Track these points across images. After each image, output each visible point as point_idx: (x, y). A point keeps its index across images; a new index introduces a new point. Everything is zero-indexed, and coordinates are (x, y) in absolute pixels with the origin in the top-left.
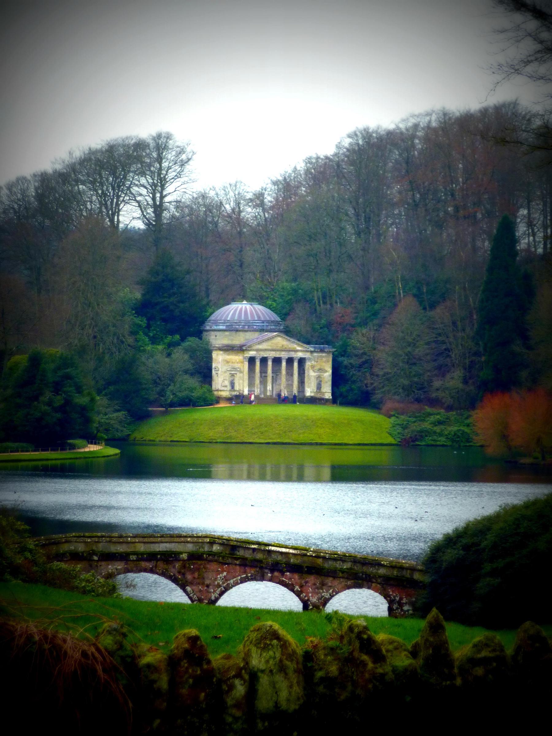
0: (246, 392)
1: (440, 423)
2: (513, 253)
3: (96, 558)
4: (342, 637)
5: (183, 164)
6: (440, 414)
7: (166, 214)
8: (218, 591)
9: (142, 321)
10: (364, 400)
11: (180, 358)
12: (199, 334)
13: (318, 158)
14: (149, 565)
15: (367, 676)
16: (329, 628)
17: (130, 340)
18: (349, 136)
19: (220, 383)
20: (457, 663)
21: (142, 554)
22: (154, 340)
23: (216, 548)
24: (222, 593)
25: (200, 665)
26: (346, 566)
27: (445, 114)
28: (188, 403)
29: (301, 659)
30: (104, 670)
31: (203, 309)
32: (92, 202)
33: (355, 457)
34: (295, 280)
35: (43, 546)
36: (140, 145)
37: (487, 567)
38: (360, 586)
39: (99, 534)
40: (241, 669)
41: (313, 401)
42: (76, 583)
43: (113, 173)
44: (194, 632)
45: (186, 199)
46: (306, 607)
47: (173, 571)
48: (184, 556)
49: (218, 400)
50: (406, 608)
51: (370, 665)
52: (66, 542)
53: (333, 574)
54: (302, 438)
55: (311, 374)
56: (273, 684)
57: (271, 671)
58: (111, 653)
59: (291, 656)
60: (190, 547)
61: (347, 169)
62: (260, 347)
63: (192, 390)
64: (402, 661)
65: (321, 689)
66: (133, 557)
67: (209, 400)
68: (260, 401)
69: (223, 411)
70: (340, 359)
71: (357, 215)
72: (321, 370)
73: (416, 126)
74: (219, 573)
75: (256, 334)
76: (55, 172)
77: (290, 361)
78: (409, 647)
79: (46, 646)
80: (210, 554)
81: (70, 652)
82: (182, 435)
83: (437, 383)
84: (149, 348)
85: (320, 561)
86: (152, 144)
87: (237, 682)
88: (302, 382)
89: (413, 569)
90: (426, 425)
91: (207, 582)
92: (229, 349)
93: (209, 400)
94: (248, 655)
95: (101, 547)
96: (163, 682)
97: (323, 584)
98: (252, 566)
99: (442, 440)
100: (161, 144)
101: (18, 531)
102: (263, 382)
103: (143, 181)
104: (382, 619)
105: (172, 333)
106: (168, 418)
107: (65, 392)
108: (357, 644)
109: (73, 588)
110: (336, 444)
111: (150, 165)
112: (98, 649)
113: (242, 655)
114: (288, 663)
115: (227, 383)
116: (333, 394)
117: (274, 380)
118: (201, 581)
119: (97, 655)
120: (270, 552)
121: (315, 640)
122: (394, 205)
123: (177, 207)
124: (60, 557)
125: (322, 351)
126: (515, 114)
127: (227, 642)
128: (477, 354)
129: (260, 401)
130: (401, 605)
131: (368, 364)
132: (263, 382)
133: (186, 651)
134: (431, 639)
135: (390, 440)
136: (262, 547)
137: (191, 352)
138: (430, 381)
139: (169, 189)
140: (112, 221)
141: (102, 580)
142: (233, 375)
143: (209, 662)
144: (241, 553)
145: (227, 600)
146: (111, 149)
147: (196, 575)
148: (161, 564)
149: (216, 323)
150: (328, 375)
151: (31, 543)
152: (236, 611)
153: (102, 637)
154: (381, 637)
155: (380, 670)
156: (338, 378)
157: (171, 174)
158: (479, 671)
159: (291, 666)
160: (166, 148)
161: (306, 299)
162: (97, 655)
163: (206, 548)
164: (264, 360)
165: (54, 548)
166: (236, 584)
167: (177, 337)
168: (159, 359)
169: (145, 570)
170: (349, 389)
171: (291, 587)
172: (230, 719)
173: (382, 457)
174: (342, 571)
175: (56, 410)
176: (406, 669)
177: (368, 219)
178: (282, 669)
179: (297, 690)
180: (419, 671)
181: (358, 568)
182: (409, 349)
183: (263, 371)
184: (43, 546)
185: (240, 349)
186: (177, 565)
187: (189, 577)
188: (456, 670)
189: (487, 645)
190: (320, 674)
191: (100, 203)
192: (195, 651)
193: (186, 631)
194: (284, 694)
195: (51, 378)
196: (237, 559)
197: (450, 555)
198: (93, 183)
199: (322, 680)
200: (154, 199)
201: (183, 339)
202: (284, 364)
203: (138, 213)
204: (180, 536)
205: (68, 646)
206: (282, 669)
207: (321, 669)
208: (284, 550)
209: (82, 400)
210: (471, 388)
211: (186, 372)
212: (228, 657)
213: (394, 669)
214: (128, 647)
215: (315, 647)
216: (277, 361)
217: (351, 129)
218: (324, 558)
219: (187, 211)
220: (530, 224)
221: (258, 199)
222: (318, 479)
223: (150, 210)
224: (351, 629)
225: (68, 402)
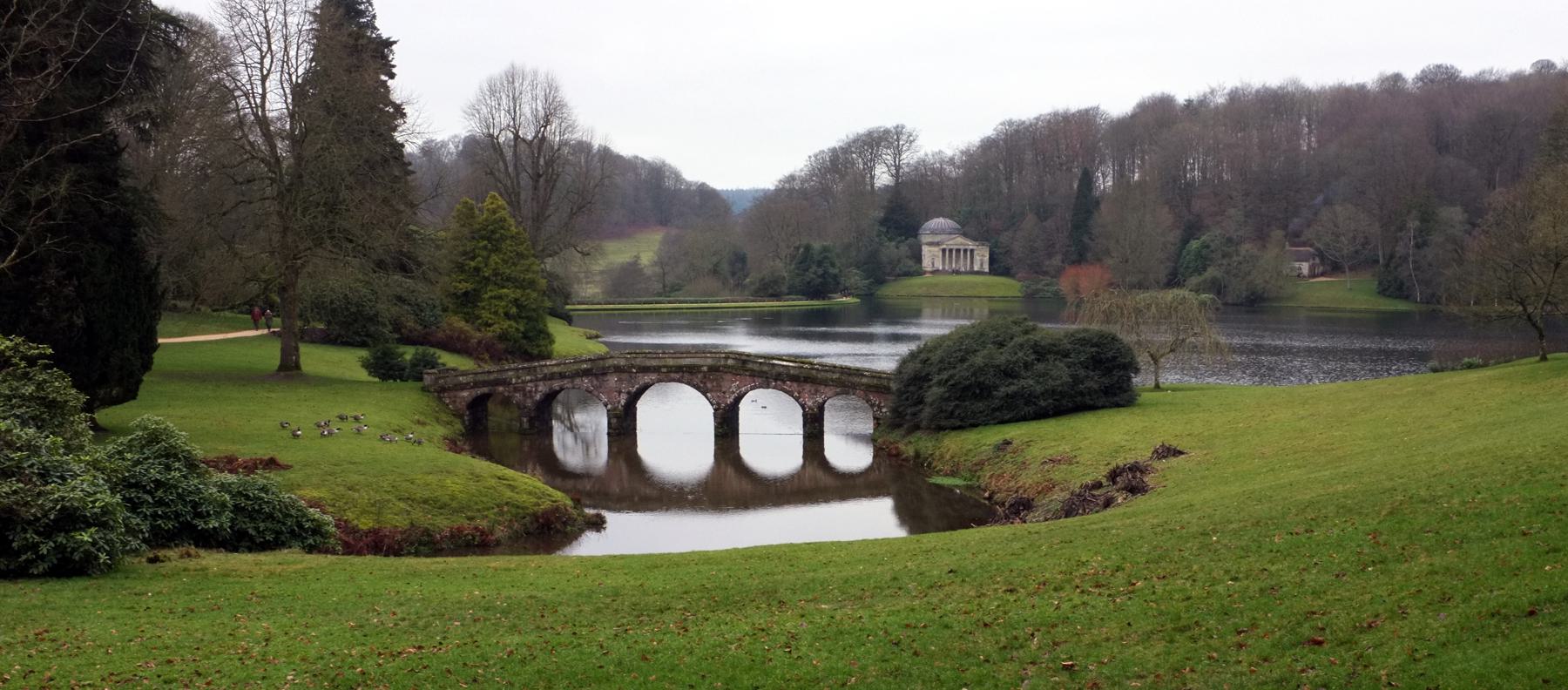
6: (1048, 279)
10: (1007, 272)
11: (904, 249)
12: (916, 236)
14: (677, 376)
19: (926, 263)
22: (891, 240)
23: (730, 362)
26: (835, 376)
28: (908, 274)
36: (887, 132)
37: (936, 379)
41: (978, 273)
53: (825, 382)
55: (977, 258)
60: (709, 362)
67: (920, 273)
69: (928, 278)
92: (931, 244)
93: (920, 273)
95: (638, 362)
97: (817, 391)
100: (899, 131)
129: (966, 273)
131: (1008, 252)
137: (910, 247)
144: (750, 366)
146: (870, 134)
150: (987, 258)
156: (992, 261)
168: (892, 250)
170: (998, 266)
171: (790, 393)
185: (938, 244)
209: (833, 271)
216: (958, 251)
217: (1001, 120)
225: (825, 272)
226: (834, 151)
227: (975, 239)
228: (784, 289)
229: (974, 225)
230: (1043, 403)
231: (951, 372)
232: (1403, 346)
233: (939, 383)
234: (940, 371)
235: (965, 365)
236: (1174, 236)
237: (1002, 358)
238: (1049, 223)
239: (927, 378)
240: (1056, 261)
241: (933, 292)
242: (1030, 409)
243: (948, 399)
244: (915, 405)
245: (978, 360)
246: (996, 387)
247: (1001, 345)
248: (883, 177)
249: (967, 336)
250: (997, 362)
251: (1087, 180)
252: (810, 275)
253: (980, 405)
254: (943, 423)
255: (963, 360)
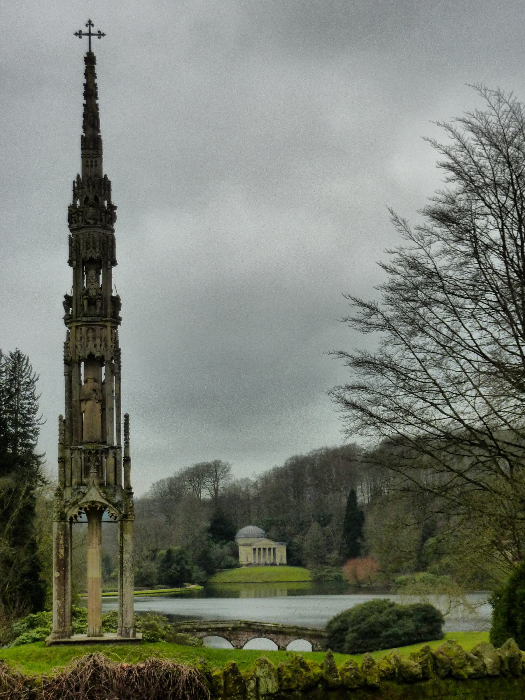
0: (253, 562)
1: (330, 572)
2: (356, 503)
3: (195, 631)
4: (292, 662)
5: (225, 473)
6: (330, 568)
7: (219, 493)
8: (244, 643)
9: (210, 535)
13: (278, 468)
14: (216, 633)
15: (303, 677)
16: (287, 658)
17: (206, 543)
18: (290, 459)
19: (242, 559)
20: (339, 671)
21: (213, 628)
22: (216, 543)
23: (243, 625)
24: (245, 643)
25: (236, 675)
26: (294, 631)
27: (327, 450)
28: (231, 567)
29: (276, 671)
30: (198, 679)
31: (237, 528)
32: (190, 489)
33: (296, 586)
34: (271, 516)
35: (174, 627)
36: (208, 466)
38: (300, 639)
39: (196, 621)
40: (253, 676)
41: (281, 564)
42: (187, 641)
43: (198, 477)
44: (233, 662)
45: (227, 486)
46: (279, 648)
47: (226, 635)
48: (230, 629)
49: (241, 566)
50: (319, 647)
51: (304, 673)
52: (183, 625)
53: (289, 634)
54: (276, 580)
55: (278, 554)
56: (266, 682)
57: (265, 677)
58: (201, 671)
59: (273, 670)
60: (232, 625)
61: (290, 472)
62: (258, 544)
63: (231, 562)
64: (317, 671)
65: (285, 683)
66: (210, 630)
67: (238, 566)
68: (259, 565)
69: (243, 570)
70: (290, 548)
71: (294, 490)
72: (282, 552)
73: (316, 455)
74: (244, 635)
75: (256, 539)
76: (175, 477)
77: (270, 549)
78: (320, 665)
79: (175, 670)
80: (240, 627)
81: (184, 672)
82: (228, 580)
83: (328, 556)
84: (214, 546)
85: (284, 629)
86: (213, 465)
87: (251, 681)
88: (275, 557)
89: (321, 631)
90: (324, 573)
91: (239, 639)
92: (246, 545)
94: (255, 670)
95: (197, 626)
96: (222, 683)
97: (285, 638)
98: (257, 632)
99: (330, 579)
100: (217, 465)
101: (164, 621)
102: (259, 557)
103: (210, 480)
104: (309, 652)
105: (223, 539)
106: (222, 573)
107: (182, 565)
108: (299, 665)
109: (186, 644)
110: (289, 582)
111: (212, 473)
112: (195, 670)
113: (253, 670)
114: (271, 673)
115: (245, 559)
116: (287, 562)
117: (263, 557)
118: (237, 638)
119: (195, 672)
120: (264, 626)
121: (282, 663)
122: (308, 486)
123: (223, 490)
124: (180, 631)
125: (282, 545)
126: (355, 449)
127: (248, 664)
128: (343, 544)
130: (317, 646)
131: (300, 549)
132: (259, 557)
133: (231, 670)
134: (328, 661)
135: (310, 579)
136: (261, 624)
137: (231, 547)
138: (325, 555)
139: (220, 482)
140: (198, 496)
141: (198, 640)
142: (247, 555)
143: (240, 674)
144: (252, 627)
145: (247, 647)
146: (197, 467)
147: (235, 636)
148: (221, 633)
149: (240, 535)
151: (169, 626)
152: (251, 652)
153: (197, 665)
154: (308, 661)
155: (308, 675)
156: (289, 554)
157: (221, 477)
158: (348, 674)
159: (272, 674)
160: (218, 466)
161: (275, 524)
162: (195, 672)
163: (239, 625)
164: (259, 549)
165: (178, 628)
166: (251, 639)
167: (225, 541)
169: (215, 635)
170: (293, 559)
172: (249, 697)
173: (307, 586)
174: (293, 633)
175: (178, 572)
176: (319, 674)
177: (298, 492)
178: (269, 675)
179: (276, 684)
180: (324, 675)
181: (299, 631)
182: (317, 543)
183: (259, 553)
184: (174, 627)
185: (250, 545)
186: (227, 633)
187: (232, 637)
188: (339, 674)
189: (351, 663)
190: (284, 677)
191: (194, 489)
192: (234, 670)
193: (230, 661)
194: (270, 686)
195: (175, 559)
196: (251, 629)
197: (336, 625)
198: (190, 481)
199: (286, 679)
200: (214, 487)
201: (227, 542)
202: (267, 550)
203: (208, 493)
204: (228, 621)
205: (183, 669)
206: (269, 675)
207: (284, 675)
208: (269, 625)
209: (188, 567)
210: (341, 557)
211: (229, 555)
212: (247, 672)
213: (314, 674)
214: (208, 668)
215: (282, 666)
216: (264, 549)
218: (286, 628)
219: (227, 491)
220: (362, 492)
221: (255, 485)
222: (282, 595)
223: (213, 491)
224: (296, 658)
225: (183, 568)
226: (171, 480)
227: (276, 541)
228: (155, 581)
229: (274, 529)
230: (403, 639)
231: (359, 626)
232: (70, 552)
233: (353, 631)
234: (352, 626)
235: (365, 622)
236: (417, 535)
237: (382, 618)
238: (329, 528)
239: (346, 629)
240: (335, 554)
241: (249, 579)
242: (398, 642)
243: (358, 639)
244: (339, 642)
245: (372, 619)
246: (381, 632)
247: (380, 612)
248: (206, 494)
249: (364, 608)
250: (380, 620)
251: (353, 497)
252: (172, 571)
253: (373, 641)
254: (356, 650)
255: (364, 620)
